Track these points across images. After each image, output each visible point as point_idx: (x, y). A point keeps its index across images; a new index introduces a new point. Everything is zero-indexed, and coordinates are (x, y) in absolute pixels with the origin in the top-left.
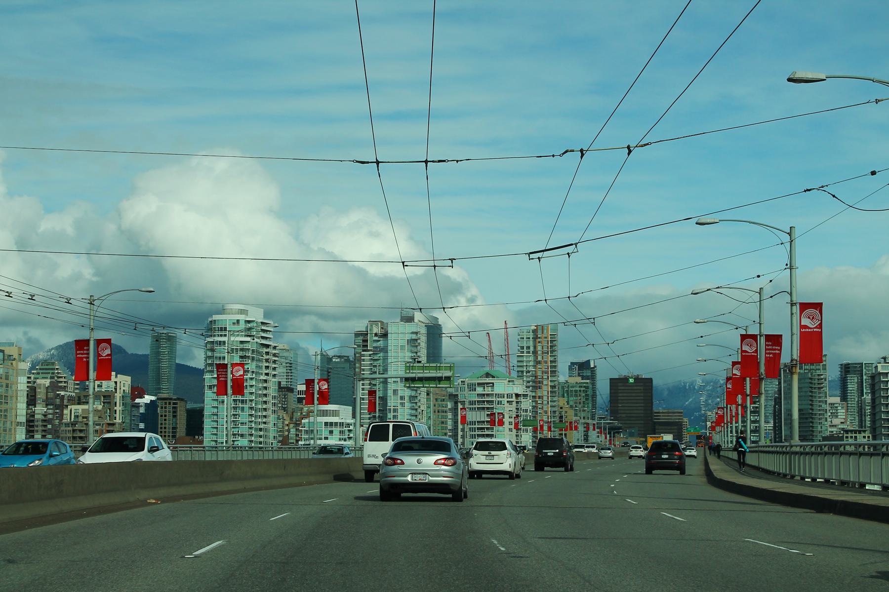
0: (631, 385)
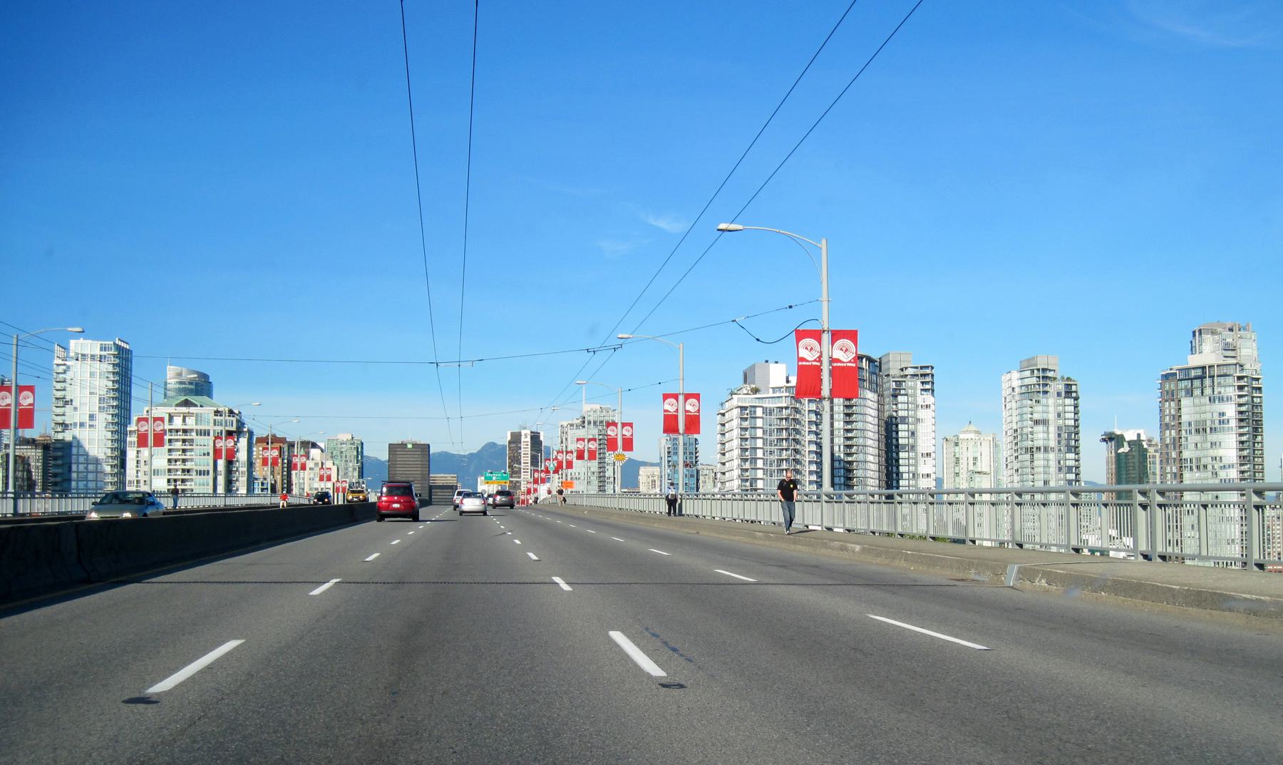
0: (410, 450)
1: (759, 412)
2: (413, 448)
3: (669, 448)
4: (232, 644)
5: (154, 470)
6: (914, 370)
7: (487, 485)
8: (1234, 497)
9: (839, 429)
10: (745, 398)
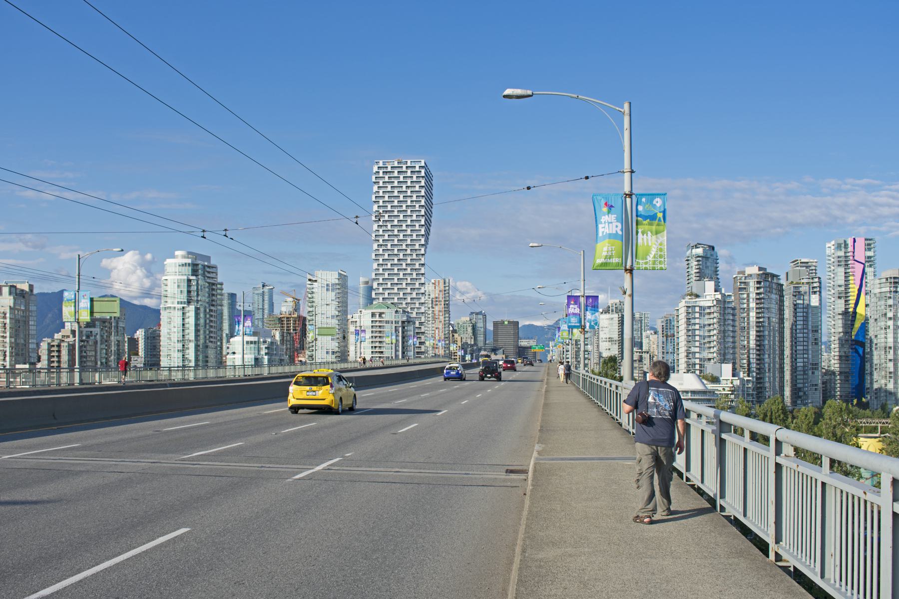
1: (697, 309)
2: (508, 324)
3: (663, 326)
4: (463, 403)
5: (383, 165)
6: (808, 279)
7: (610, 343)
8: (267, 366)
9: (753, 317)
10: (690, 301)
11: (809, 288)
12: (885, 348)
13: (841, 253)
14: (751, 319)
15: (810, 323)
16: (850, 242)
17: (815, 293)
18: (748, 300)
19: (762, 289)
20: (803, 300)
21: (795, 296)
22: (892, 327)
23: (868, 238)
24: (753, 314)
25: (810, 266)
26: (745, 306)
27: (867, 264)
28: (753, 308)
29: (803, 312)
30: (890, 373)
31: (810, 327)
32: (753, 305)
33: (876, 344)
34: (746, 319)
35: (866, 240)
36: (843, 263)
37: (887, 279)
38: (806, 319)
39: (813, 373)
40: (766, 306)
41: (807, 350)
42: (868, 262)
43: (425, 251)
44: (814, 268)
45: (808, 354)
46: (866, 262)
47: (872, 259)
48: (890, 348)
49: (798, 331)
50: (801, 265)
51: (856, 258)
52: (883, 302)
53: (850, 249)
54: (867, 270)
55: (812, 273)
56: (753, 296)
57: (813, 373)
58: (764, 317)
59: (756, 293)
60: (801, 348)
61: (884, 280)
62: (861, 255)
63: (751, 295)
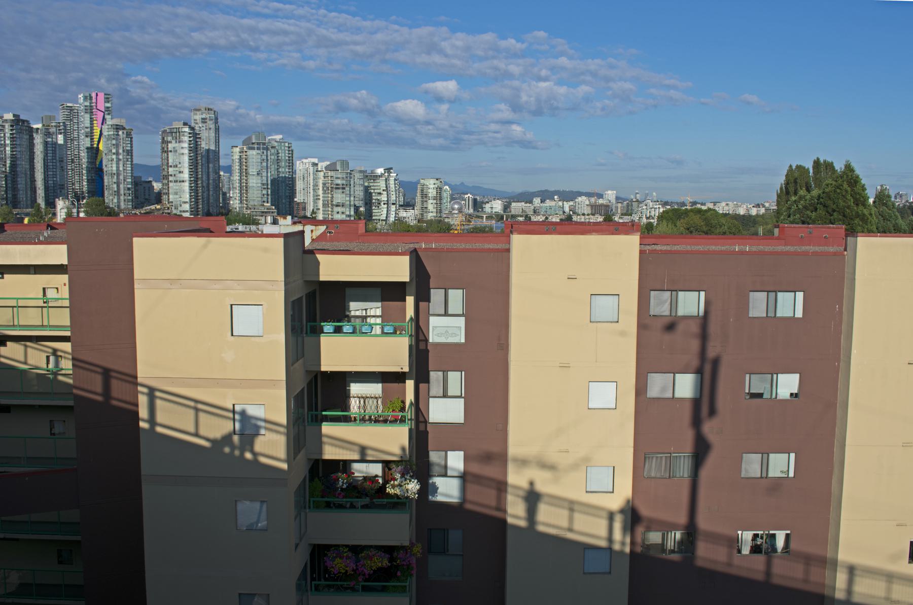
11: (56, 130)
12: (112, 174)
13: (87, 104)
14: (7, 152)
15: (58, 155)
16: (94, 95)
17: (61, 133)
18: (5, 139)
19: (15, 131)
20: (52, 138)
21: (46, 135)
22: (115, 160)
23: (107, 93)
24: (8, 149)
25: (73, 110)
26: (3, 142)
27: (106, 113)
28: (8, 144)
29: (52, 147)
30: (115, 192)
31: (58, 158)
32: (8, 142)
33: (106, 171)
34: (3, 152)
35: (105, 94)
36: (89, 111)
37: (112, 125)
38: (54, 152)
39: (61, 191)
40: (18, 143)
41: (56, 175)
42: (107, 111)
43: (747, 399)
44: (76, 111)
45: (56, 178)
46: (105, 111)
47: (110, 109)
48: (114, 174)
49: (49, 161)
50: (67, 108)
51: (98, 108)
52: (109, 142)
53: (94, 101)
54: (107, 117)
55: (75, 115)
56: (8, 135)
57: (61, 191)
58: (16, 151)
59: (10, 134)
60: (51, 173)
61: (110, 126)
62: (102, 105)
63: (6, 135)
